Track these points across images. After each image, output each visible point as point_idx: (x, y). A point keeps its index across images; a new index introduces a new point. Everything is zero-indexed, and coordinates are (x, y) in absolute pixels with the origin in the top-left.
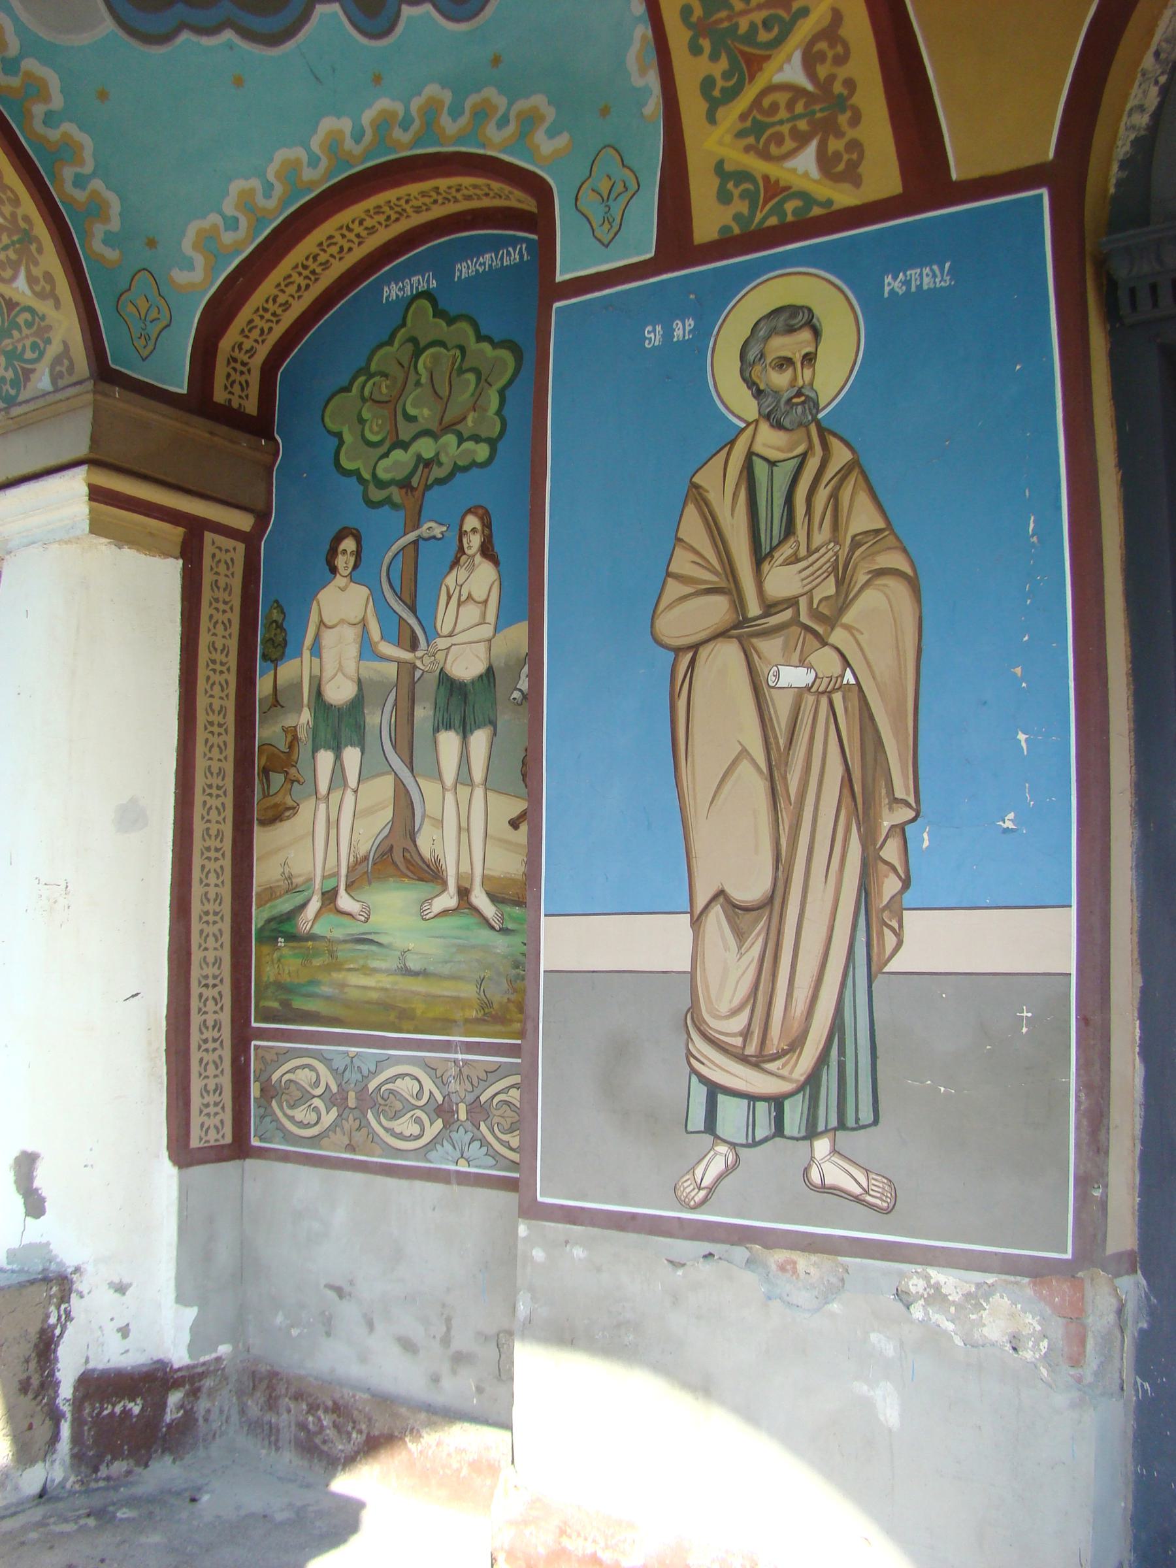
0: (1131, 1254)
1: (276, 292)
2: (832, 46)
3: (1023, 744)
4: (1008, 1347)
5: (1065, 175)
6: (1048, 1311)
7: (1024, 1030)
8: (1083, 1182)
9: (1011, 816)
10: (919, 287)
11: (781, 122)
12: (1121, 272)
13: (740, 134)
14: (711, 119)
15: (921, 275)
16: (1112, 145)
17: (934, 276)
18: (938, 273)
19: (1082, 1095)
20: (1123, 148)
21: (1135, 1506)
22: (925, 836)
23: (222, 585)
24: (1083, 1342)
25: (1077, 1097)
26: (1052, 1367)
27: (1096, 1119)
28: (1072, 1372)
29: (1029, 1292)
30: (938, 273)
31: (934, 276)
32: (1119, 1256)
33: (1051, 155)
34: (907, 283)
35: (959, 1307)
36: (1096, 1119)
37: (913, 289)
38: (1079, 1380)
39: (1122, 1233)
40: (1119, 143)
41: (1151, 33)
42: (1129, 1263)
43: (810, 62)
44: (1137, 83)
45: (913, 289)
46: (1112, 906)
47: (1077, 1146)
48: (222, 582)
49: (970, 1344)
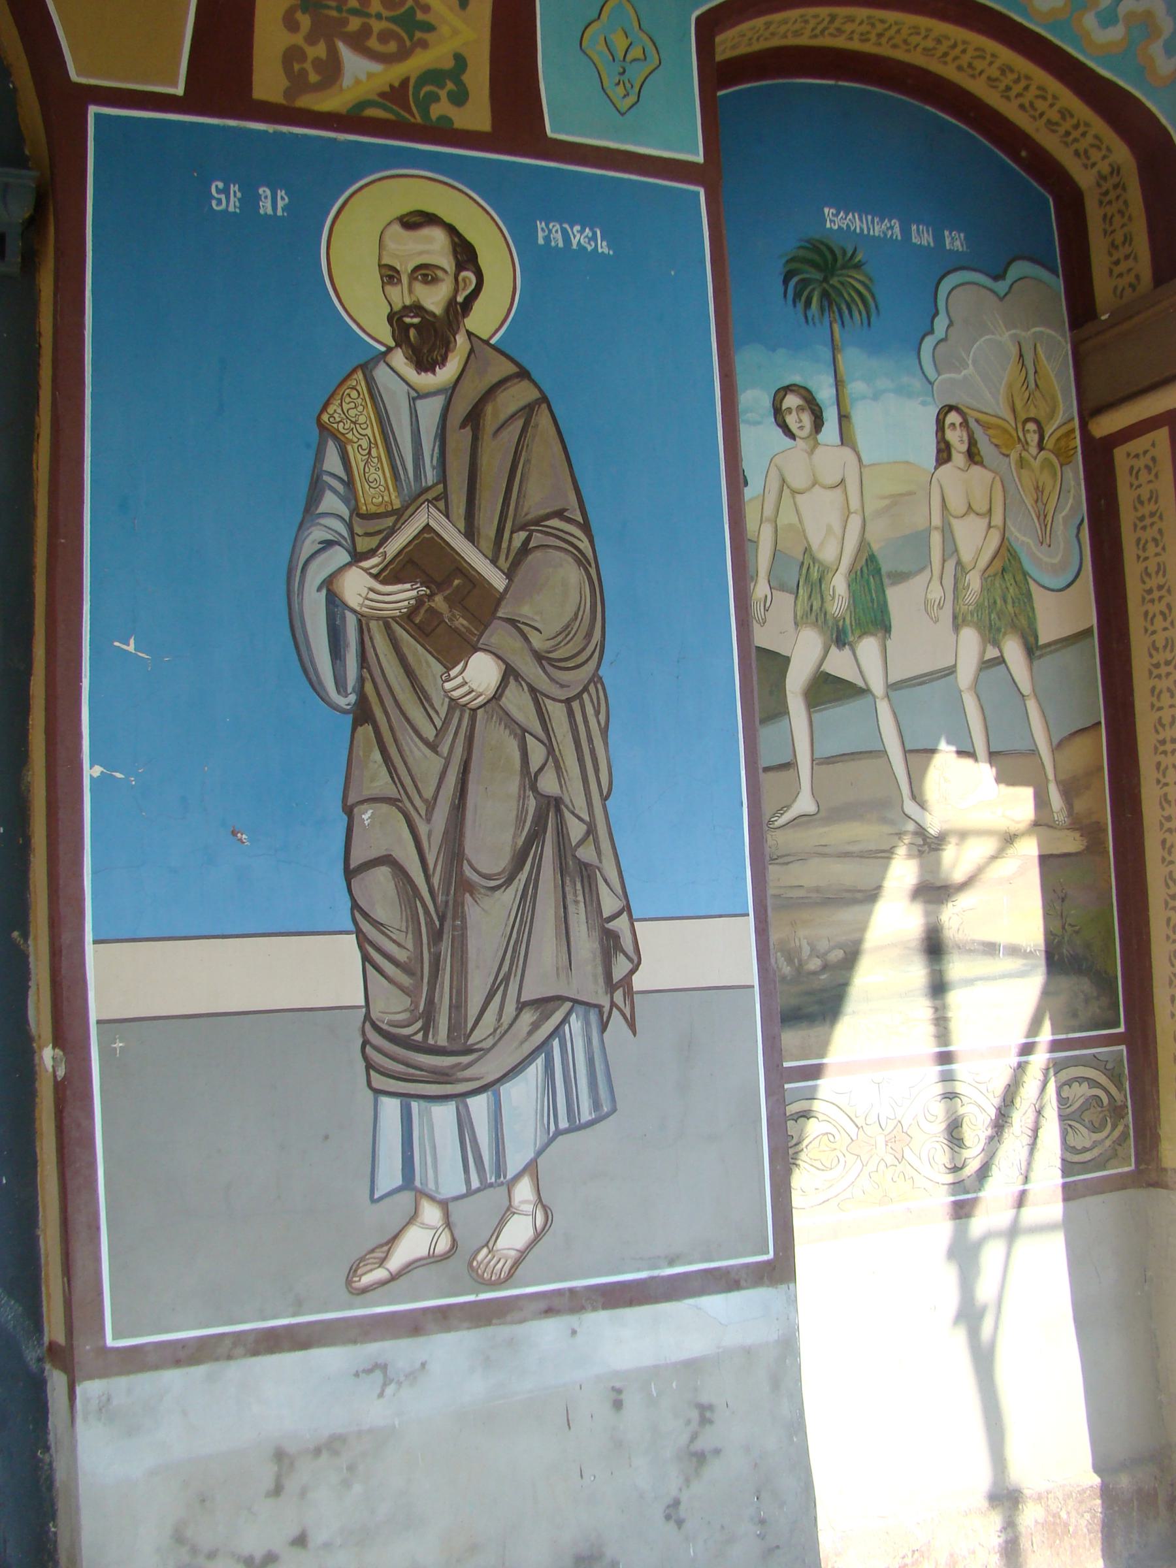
1: (1143, 565)
2: (303, 73)
11: (379, 17)
13: (429, 28)
14: (460, 61)
23: (1056, 117)
43: (332, 70)
48: (1053, 115)
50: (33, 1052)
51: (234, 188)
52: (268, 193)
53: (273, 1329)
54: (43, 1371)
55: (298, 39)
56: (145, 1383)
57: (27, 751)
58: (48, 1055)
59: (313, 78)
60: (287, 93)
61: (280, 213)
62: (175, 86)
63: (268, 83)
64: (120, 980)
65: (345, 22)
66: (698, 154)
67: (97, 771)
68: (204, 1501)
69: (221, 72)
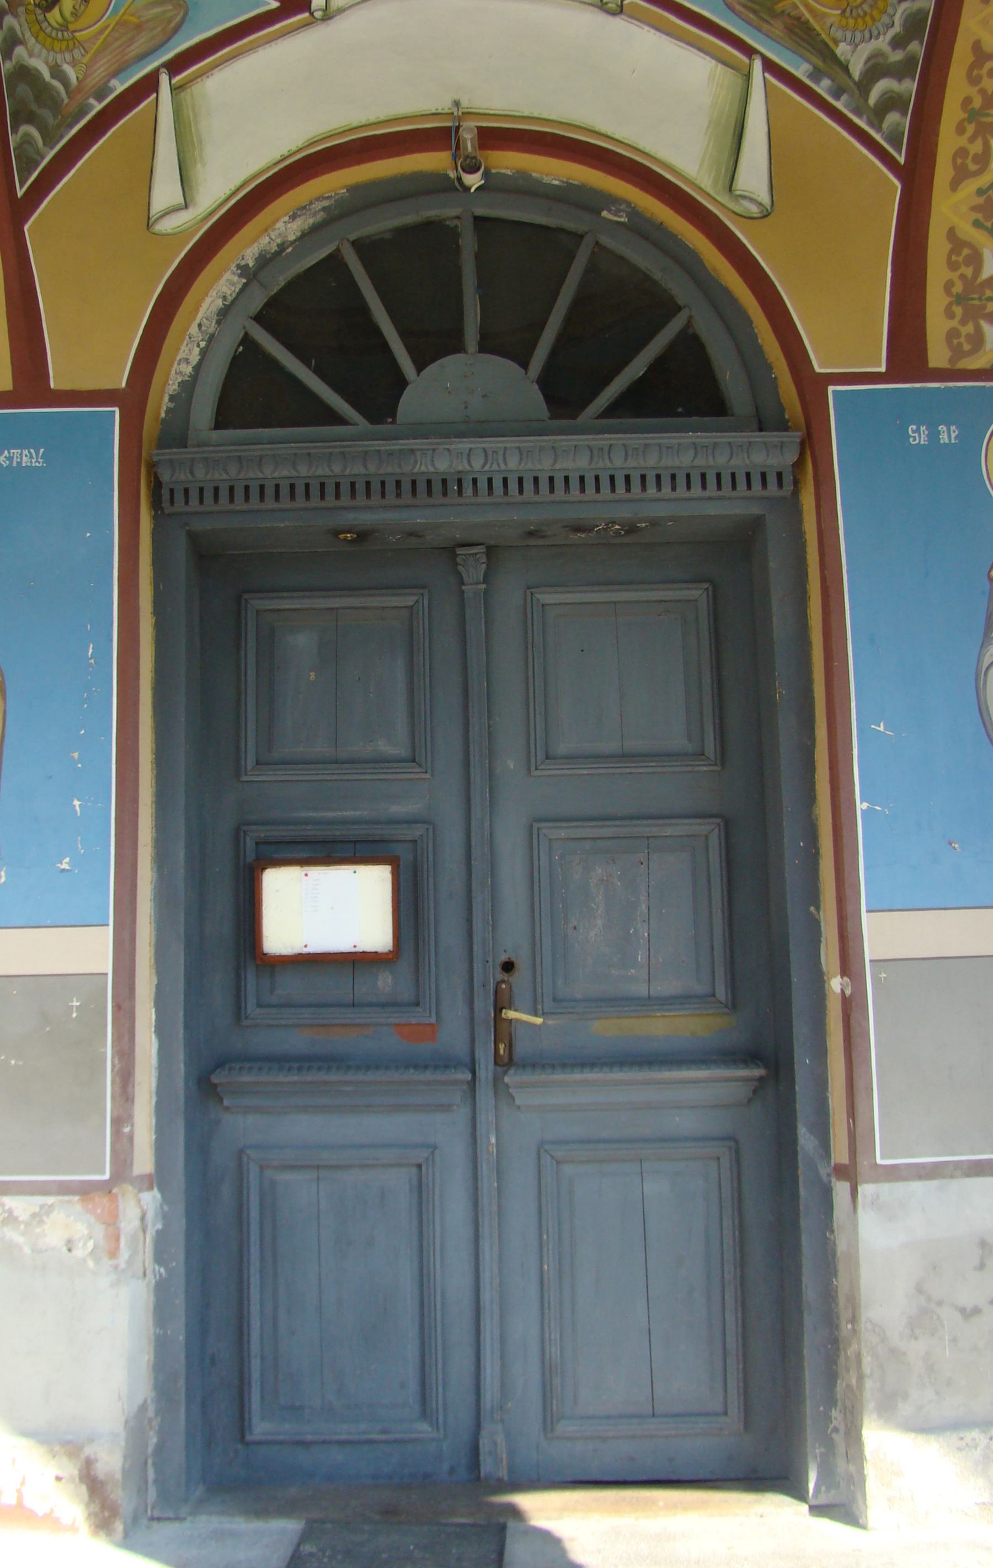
0: (150, 1176)
2: (960, 345)
3: (78, 808)
4: (65, 1249)
5: (132, 400)
6: (93, 1219)
7: (74, 1015)
8: (118, 1122)
9: (67, 860)
10: (19, 463)
12: (165, 477)
15: (21, 454)
16: (166, 383)
17: (32, 457)
18: (34, 455)
19: (116, 1061)
20: (173, 387)
21: (155, 1357)
22: (3, 873)
24: (117, 1239)
25: (112, 1062)
26: (97, 1261)
27: (125, 1077)
28: (110, 1262)
29: (78, 1207)
30: (34, 455)
31: (32, 457)
32: (142, 1177)
33: (124, 385)
34: (10, 459)
35: (27, 1224)
36: (125, 1077)
37: (15, 464)
38: (116, 1267)
39: (144, 1162)
40: (170, 382)
41: (197, 310)
42: (148, 1182)
43: (978, 340)
44: (185, 342)
45: (15, 464)
46: (138, 924)
47: (113, 1097)
49: (36, 1250)
50: (824, 981)
51: (923, 428)
52: (945, 429)
53: (980, 1161)
54: (830, 1182)
55: (954, 323)
56: (900, 1188)
57: (815, 795)
58: (836, 984)
59: (967, 347)
60: (951, 360)
61: (953, 441)
62: (880, 366)
63: (938, 356)
64: (885, 935)
65: (984, 307)
66: (900, 153)
67: (865, 806)
68: (935, 1268)
69: (907, 354)
